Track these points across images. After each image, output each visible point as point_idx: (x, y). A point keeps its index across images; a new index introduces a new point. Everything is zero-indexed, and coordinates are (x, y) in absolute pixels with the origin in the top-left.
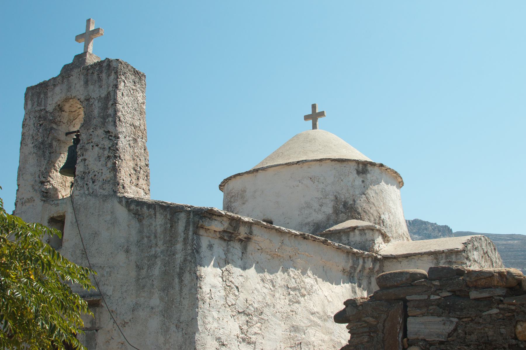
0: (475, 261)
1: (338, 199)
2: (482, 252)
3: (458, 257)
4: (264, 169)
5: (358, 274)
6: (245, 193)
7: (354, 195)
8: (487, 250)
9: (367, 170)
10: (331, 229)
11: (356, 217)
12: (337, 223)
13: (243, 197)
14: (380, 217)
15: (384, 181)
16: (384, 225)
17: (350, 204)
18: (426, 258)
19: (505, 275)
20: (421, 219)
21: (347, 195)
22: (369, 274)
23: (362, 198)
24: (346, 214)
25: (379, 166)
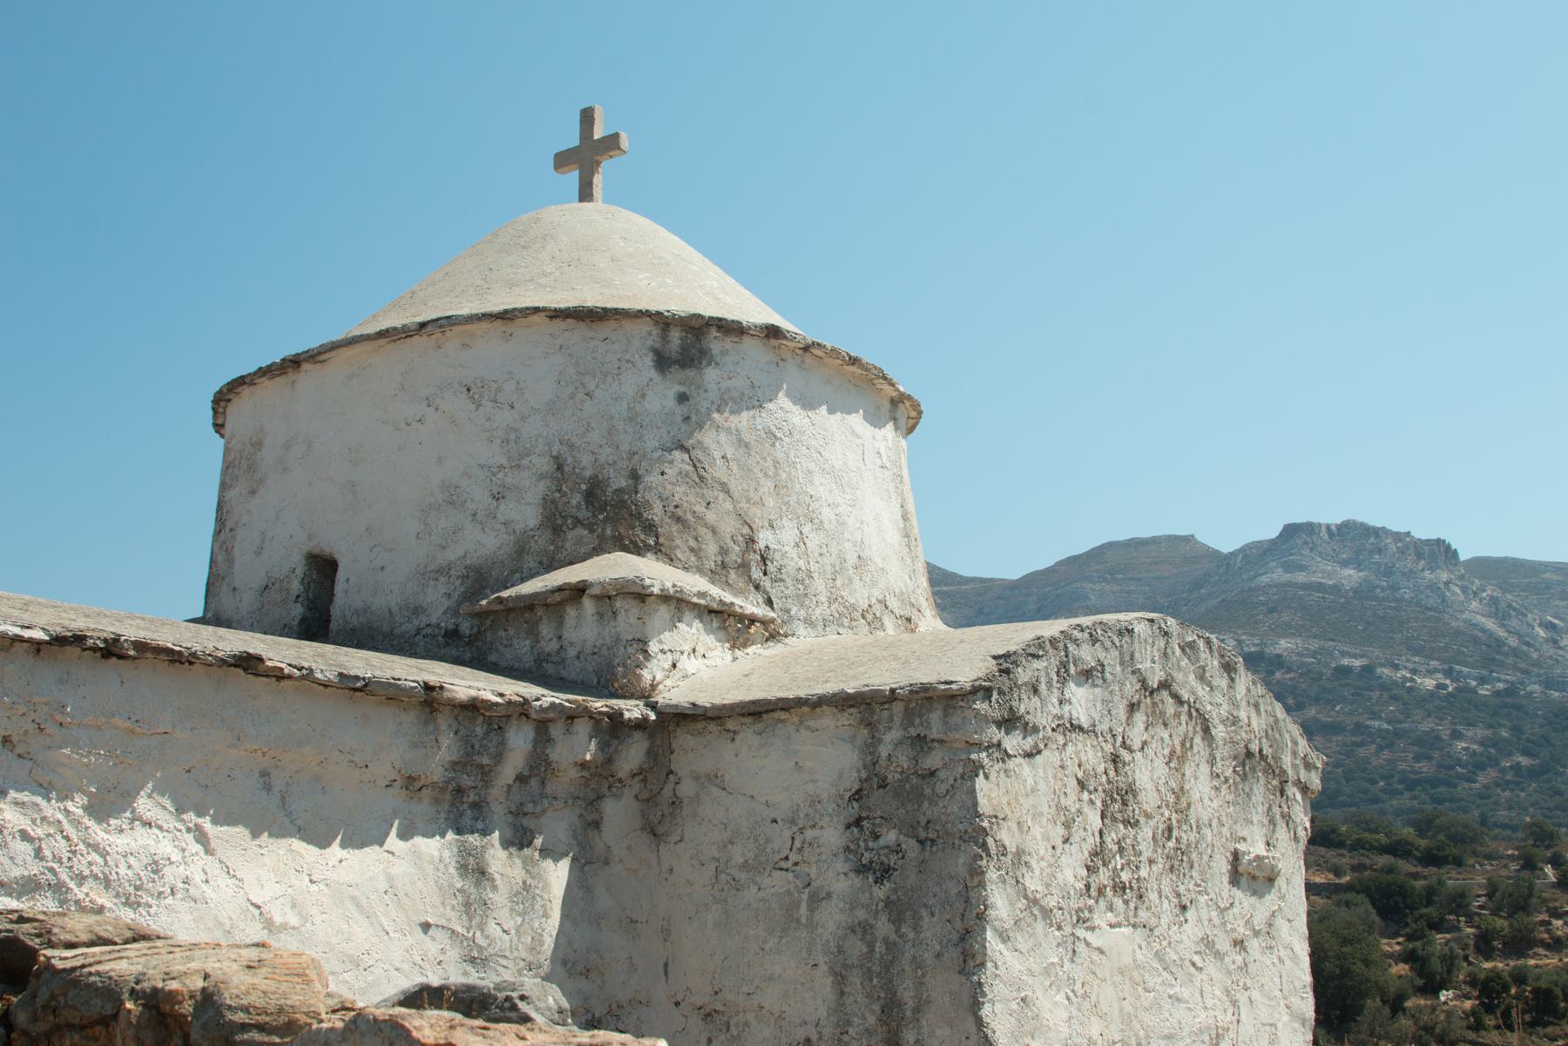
1: (566, 469)
2: (1131, 687)
3: (955, 719)
4: (312, 357)
5: (509, 792)
6: (260, 450)
7: (634, 453)
10: (505, 594)
11: (634, 543)
12: (550, 565)
13: (252, 468)
14: (751, 541)
15: (788, 395)
17: (618, 490)
18: (828, 720)
19: (180, 1019)
20: (1366, 522)
21: (606, 454)
23: (671, 462)
24: (592, 531)
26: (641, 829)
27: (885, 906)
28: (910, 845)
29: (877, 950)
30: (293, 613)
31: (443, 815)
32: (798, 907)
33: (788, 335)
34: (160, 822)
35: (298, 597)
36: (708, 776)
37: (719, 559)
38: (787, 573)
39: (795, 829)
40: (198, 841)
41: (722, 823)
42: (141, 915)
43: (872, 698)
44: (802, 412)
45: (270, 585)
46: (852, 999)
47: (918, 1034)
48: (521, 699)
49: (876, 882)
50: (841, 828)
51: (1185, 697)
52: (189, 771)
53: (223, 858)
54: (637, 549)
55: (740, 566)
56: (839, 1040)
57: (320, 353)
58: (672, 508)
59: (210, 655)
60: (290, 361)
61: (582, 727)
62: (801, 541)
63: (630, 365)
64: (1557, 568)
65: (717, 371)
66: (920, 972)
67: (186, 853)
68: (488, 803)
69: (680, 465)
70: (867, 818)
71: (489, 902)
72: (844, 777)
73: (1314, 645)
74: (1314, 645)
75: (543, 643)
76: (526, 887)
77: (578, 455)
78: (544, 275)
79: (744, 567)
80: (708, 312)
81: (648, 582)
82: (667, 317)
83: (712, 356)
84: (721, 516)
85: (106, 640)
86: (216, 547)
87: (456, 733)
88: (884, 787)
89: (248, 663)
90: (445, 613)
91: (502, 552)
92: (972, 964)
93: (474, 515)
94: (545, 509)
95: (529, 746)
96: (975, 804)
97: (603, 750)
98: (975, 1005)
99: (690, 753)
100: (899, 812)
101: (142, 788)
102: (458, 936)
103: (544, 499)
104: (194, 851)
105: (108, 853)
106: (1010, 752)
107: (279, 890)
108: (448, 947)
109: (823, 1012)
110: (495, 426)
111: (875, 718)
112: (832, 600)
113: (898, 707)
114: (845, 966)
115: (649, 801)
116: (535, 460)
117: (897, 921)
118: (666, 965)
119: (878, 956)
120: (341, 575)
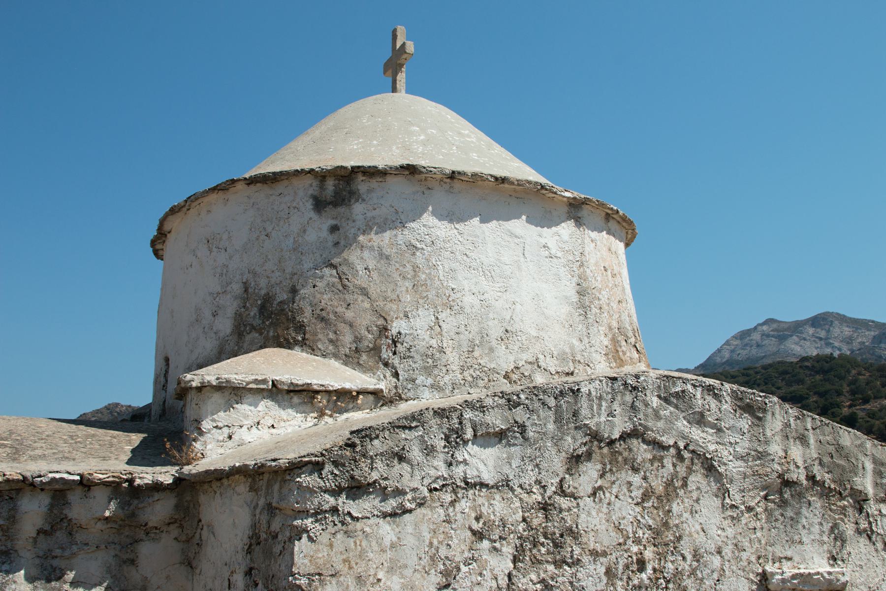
11: (287, 340)
15: (434, 213)
17: (281, 302)
24: (261, 334)
26: (180, 563)
33: (424, 170)
51: (668, 440)
55: (371, 350)
58: (318, 312)
63: (296, 210)
65: (363, 205)
79: (375, 350)
80: (350, 163)
94: (235, 320)
97: (123, 509)
103: (236, 313)
106: (355, 514)
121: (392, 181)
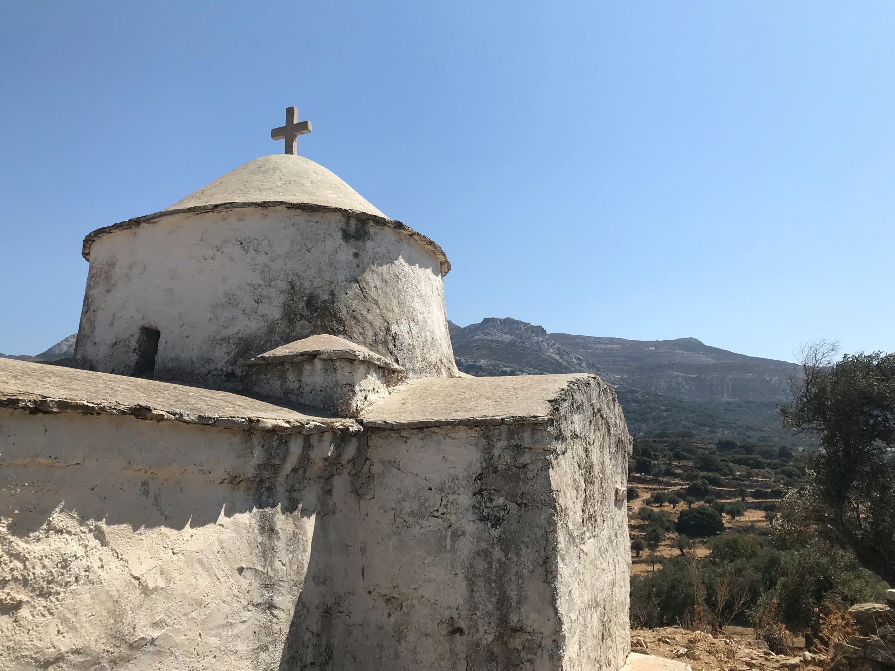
0: (575, 436)
1: (296, 288)
2: (590, 412)
3: (538, 436)
4: (148, 219)
6: (114, 269)
7: (332, 282)
8: (600, 405)
9: (366, 233)
10: (267, 355)
12: (288, 340)
13: (108, 278)
14: (388, 330)
15: (403, 258)
16: (395, 347)
18: (462, 433)
21: (317, 282)
22: (326, 469)
24: (310, 322)
25: (395, 227)
27: (498, 541)
28: (512, 506)
29: (494, 566)
30: (131, 359)
31: (251, 497)
32: (445, 538)
34: (69, 529)
35: (135, 350)
36: (390, 462)
37: (374, 338)
38: (405, 346)
39: (443, 494)
40: (96, 537)
41: (398, 489)
42: (51, 602)
43: (490, 424)
44: (410, 267)
45: (118, 343)
46: (478, 594)
47: (519, 617)
48: (300, 425)
49: (492, 527)
50: (471, 495)
52: (93, 489)
53: (115, 547)
54: (334, 333)
56: (471, 618)
57: (153, 218)
59: (114, 409)
60: (134, 221)
61: (328, 437)
62: (409, 331)
64: (582, 338)
66: (520, 581)
67: (88, 549)
68: (275, 486)
69: (355, 290)
70: (486, 489)
71: (275, 548)
72: (473, 466)
73: (494, 362)
74: (494, 362)
75: (289, 383)
76: (295, 534)
77: (302, 281)
78: (278, 187)
79: (385, 343)
81: (357, 353)
82: (350, 213)
83: (370, 235)
84: (375, 317)
85: (35, 402)
86: (84, 320)
87: (262, 447)
88: (496, 473)
89: (141, 412)
90: (226, 363)
91: (260, 331)
92: (551, 577)
93: (244, 311)
95: (300, 451)
96: (550, 485)
98: (553, 600)
99: (380, 450)
100: (505, 487)
101: (57, 506)
102: (258, 573)
104: (93, 546)
105: (27, 559)
107: (151, 563)
108: (253, 581)
109: (461, 601)
110: (256, 263)
111: (491, 434)
112: (423, 360)
113: (504, 428)
114: (474, 575)
115: (355, 475)
116: (279, 283)
117: (506, 551)
118: (363, 570)
119: (494, 570)
120: (162, 340)
121: (387, 230)
